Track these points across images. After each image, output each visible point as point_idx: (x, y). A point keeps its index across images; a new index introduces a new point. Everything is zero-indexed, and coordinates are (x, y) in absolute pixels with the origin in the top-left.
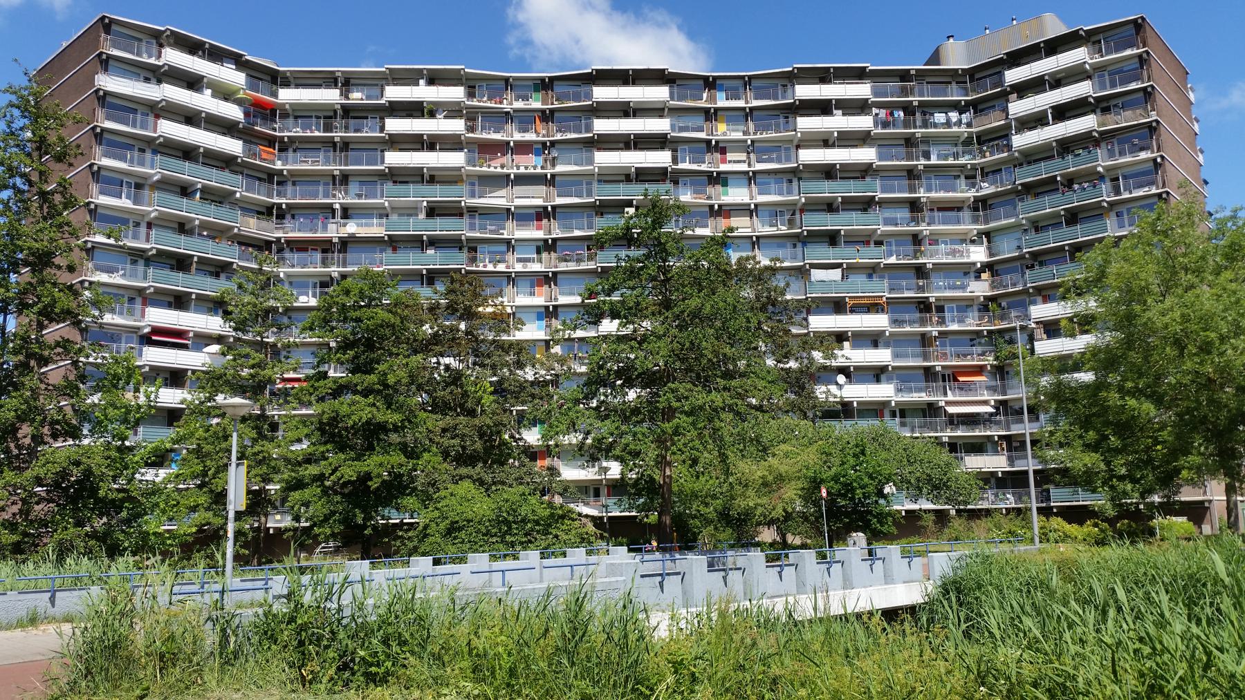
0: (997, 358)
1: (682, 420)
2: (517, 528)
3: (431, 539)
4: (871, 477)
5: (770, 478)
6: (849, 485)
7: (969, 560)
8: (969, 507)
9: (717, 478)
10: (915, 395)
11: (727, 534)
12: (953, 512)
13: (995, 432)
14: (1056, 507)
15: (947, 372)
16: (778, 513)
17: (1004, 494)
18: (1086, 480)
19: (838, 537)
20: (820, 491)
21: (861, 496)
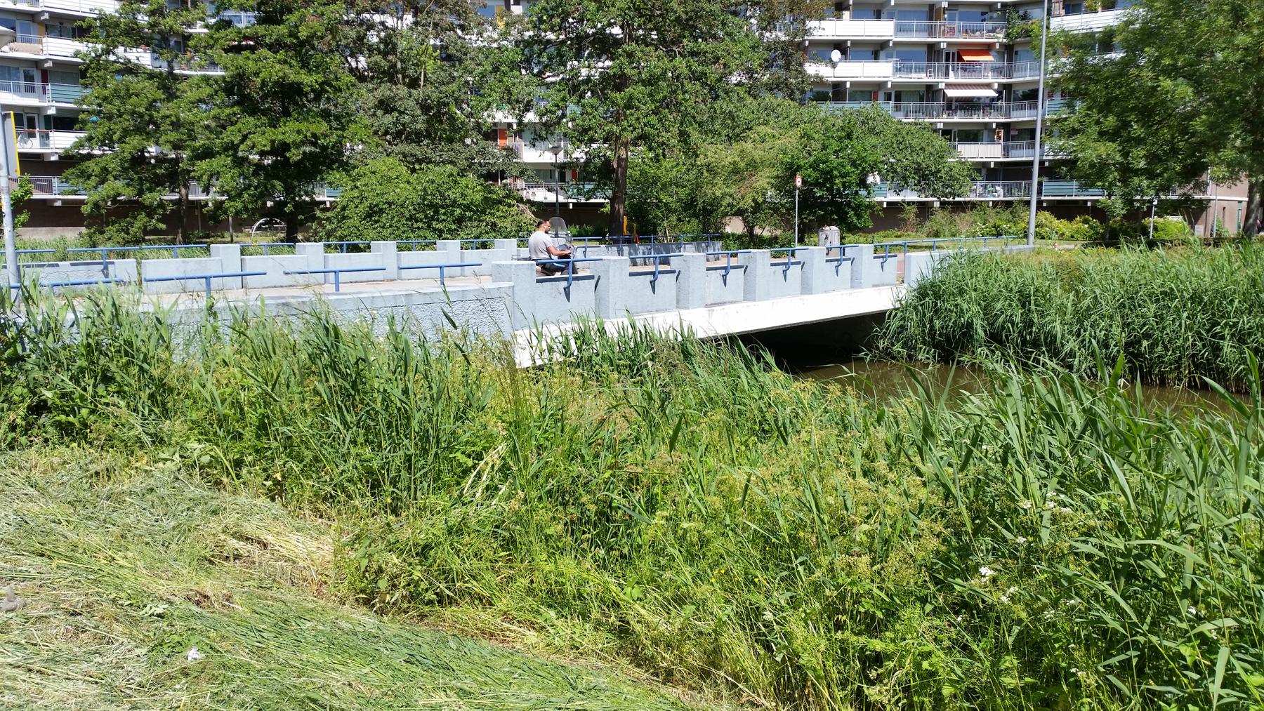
0: (1007, 36)
1: (636, 90)
2: (444, 214)
3: (349, 222)
4: (854, 164)
5: (742, 165)
6: (828, 172)
7: (952, 261)
8: (957, 199)
9: (684, 164)
10: (914, 75)
11: (693, 225)
12: (937, 205)
13: (994, 119)
14: (1047, 201)
15: (953, 50)
16: (747, 203)
17: (993, 186)
18: (1094, 174)
19: (806, 232)
20: (795, 181)
21: (840, 185)
